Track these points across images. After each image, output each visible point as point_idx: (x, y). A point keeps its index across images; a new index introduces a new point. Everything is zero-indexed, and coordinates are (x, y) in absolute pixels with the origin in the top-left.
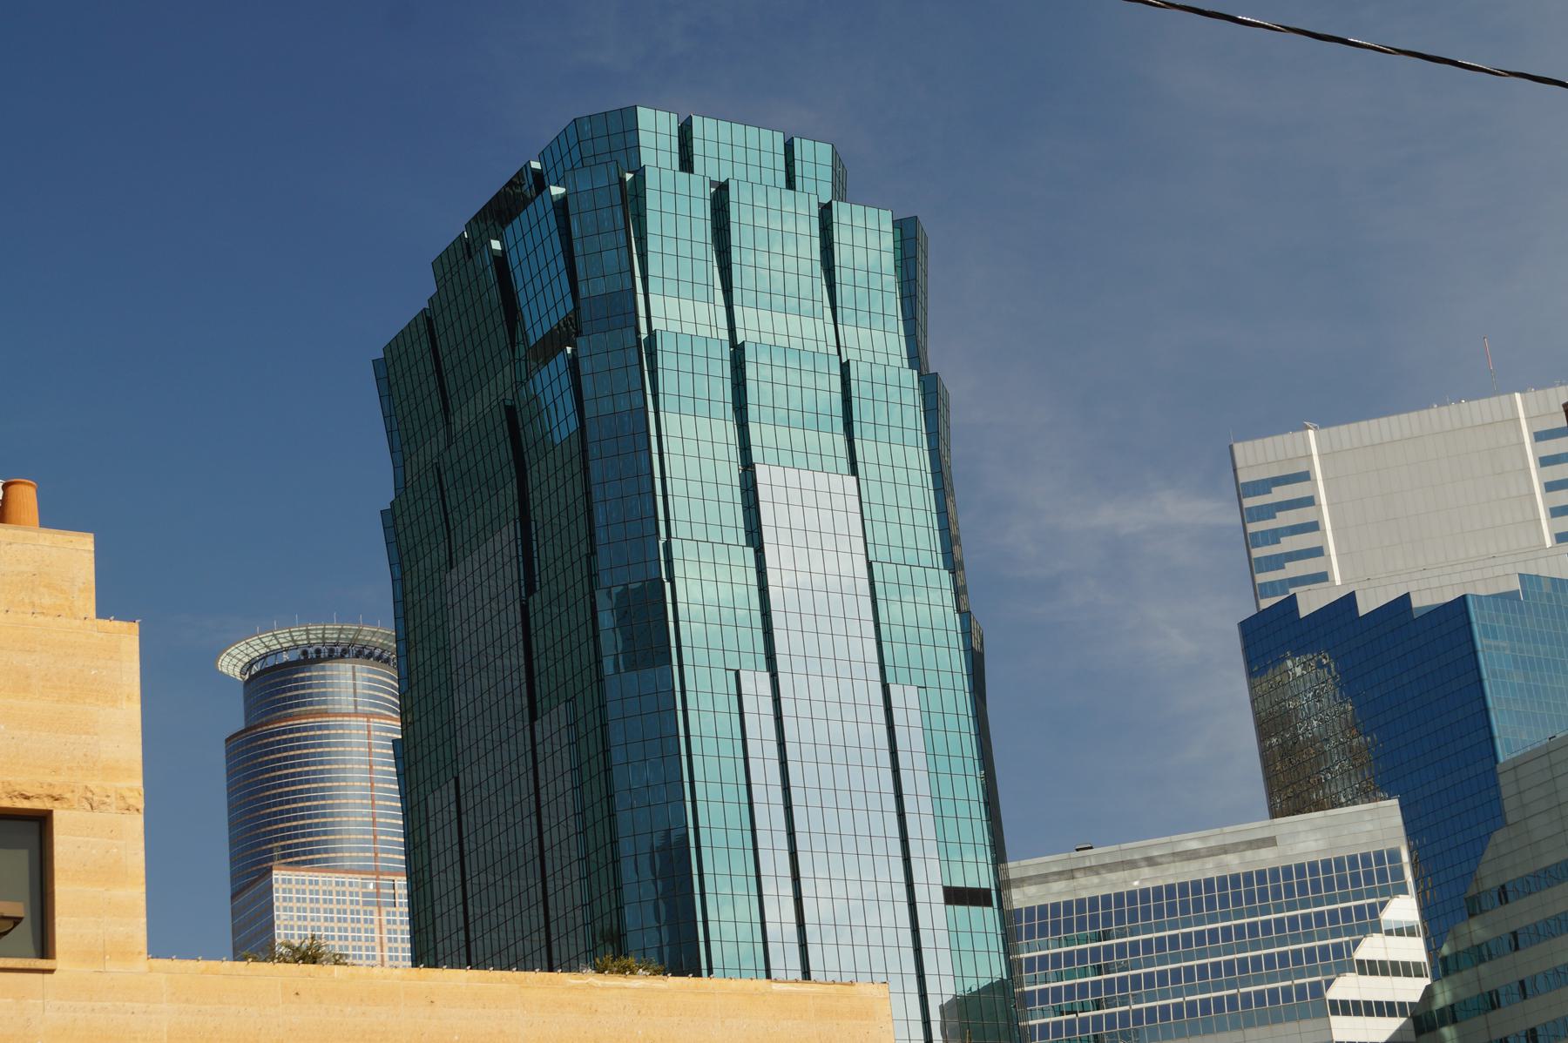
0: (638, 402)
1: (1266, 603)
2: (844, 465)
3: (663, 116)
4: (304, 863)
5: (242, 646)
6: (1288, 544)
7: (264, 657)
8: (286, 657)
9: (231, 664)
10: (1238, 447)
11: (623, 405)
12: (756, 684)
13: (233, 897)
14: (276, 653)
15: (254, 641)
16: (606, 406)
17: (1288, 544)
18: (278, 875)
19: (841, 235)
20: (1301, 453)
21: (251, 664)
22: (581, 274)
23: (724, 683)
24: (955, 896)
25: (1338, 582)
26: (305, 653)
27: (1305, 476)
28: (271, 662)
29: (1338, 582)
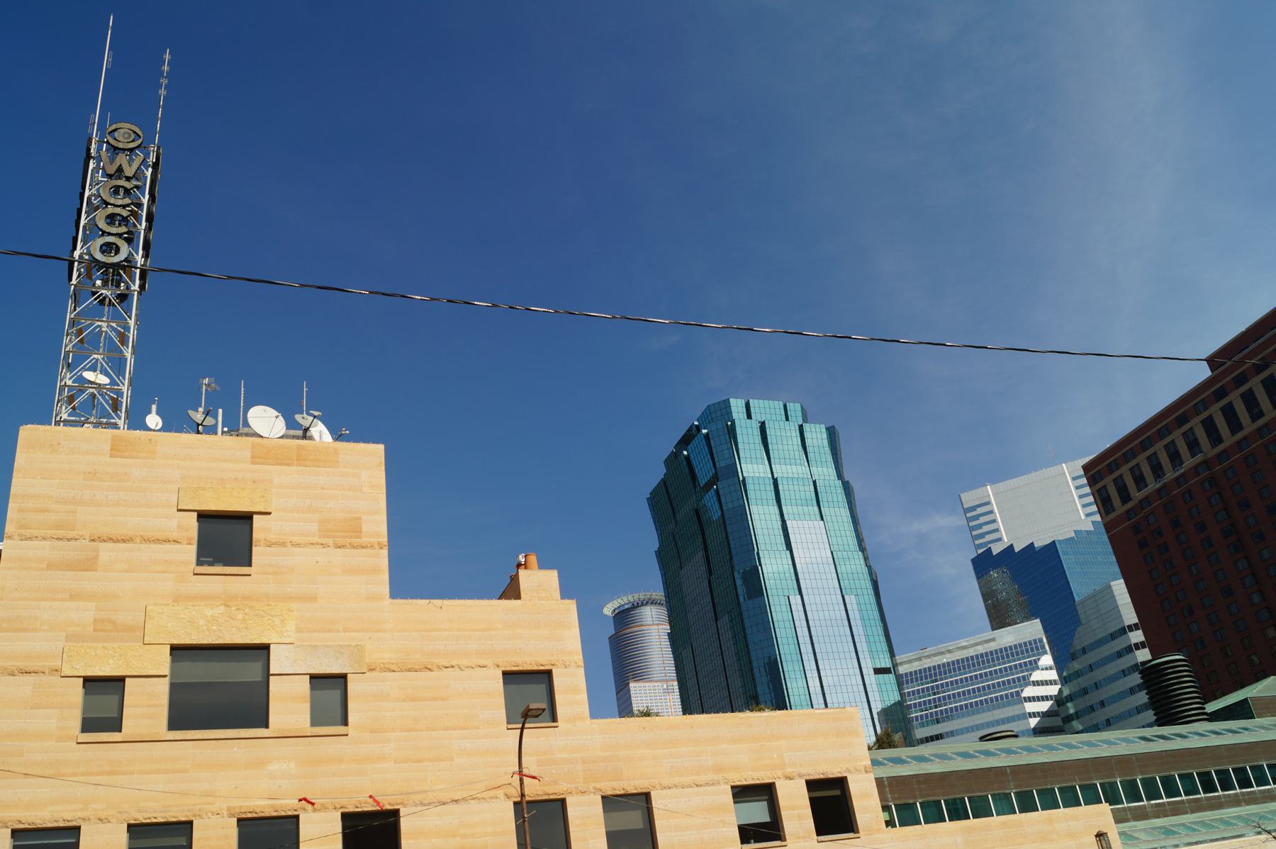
0: (742, 503)
1: (980, 551)
3: (739, 400)
4: (640, 680)
5: (611, 604)
6: (985, 529)
7: (619, 607)
8: (626, 606)
9: (608, 610)
10: (962, 495)
11: (736, 504)
12: (796, 600)
13: (617, 694)
14: (623, 605)
15: (615, 602)
16: (730, 506)
17: (985, 529)
18: (632, 685)
19: (807, 435)
20: (986, 495)
21: (614, 610)
22: (716, 460)
23: (784, 601)
24: (878, 671)
25: (1006, 541)
26: (633, 604)
27: (988, 503)
28: (621, 609)
29: (1006, 541)
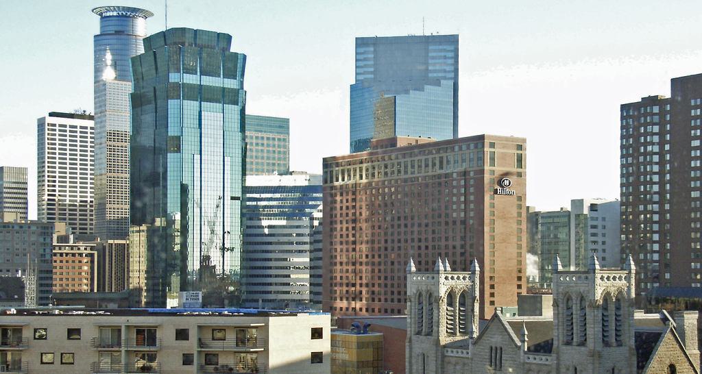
2: (221, 111)
12: (197, 157)
23: (190, 156)
24: (232, 198)
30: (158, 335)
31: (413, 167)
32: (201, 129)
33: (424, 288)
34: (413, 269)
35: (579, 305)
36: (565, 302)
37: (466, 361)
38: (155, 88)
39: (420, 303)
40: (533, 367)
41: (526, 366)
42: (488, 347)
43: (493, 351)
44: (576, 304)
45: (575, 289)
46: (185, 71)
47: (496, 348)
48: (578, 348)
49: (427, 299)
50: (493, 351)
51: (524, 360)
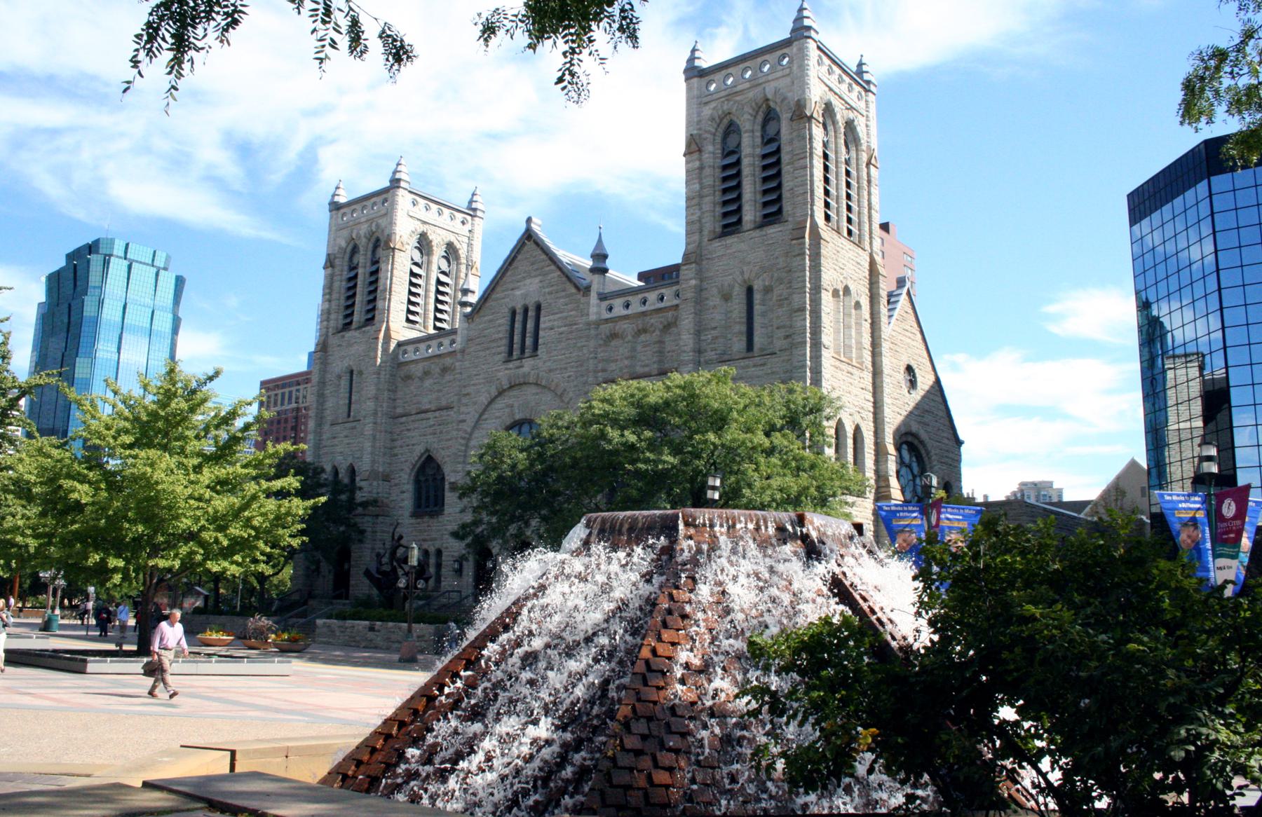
19: (160, 278)
30: (532, 50)
31: (297, 398)
32: (119, 353)
33: (364, 229)
34: (586, 789)
35: (758, 134)
36: (719, 139)
37: (448, 361)
38: (70, 305)
39: (353, 268)
40: (624, 326)
41: (606, 329)
42: (506, 311)
43: (519, 318)
44: (753, 131)
45: (751, 94)
46: (1220, 549)
47: (526, 310)
48: (757, 233)
49: (369, 253)
50: (519, 318)
51: (598, 313)
